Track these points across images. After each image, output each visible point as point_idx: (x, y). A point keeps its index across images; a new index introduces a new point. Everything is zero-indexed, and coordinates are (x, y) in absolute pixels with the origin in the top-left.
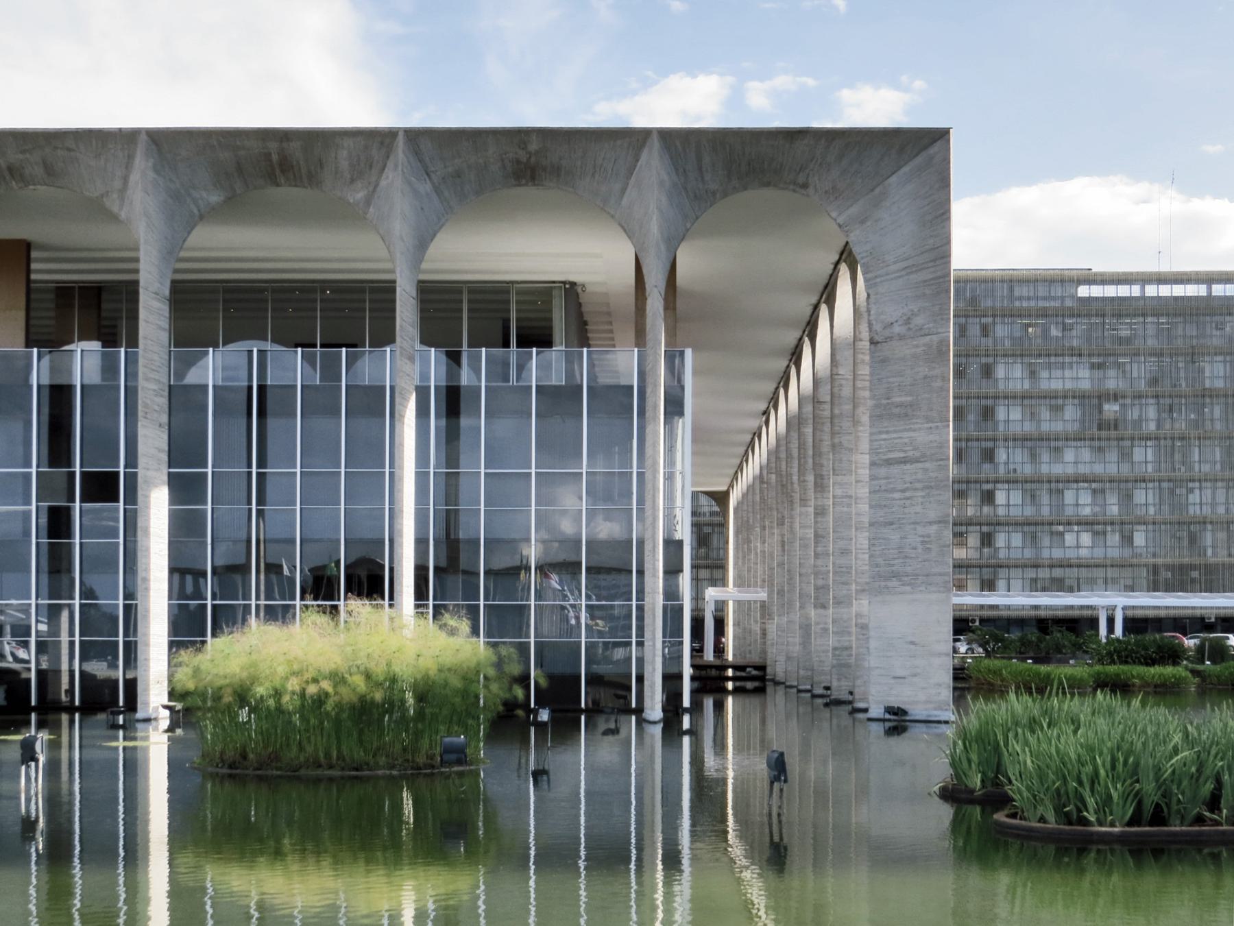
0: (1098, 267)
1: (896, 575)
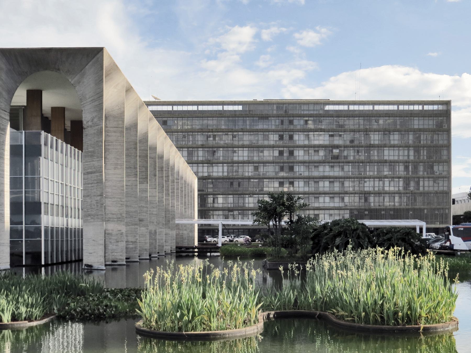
0: (331, 99)
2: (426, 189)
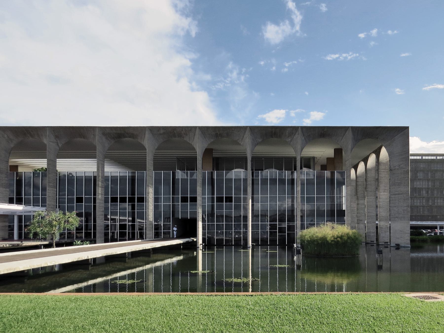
0: (380, 184)
1: (397, 217)
2: (439, 204)
